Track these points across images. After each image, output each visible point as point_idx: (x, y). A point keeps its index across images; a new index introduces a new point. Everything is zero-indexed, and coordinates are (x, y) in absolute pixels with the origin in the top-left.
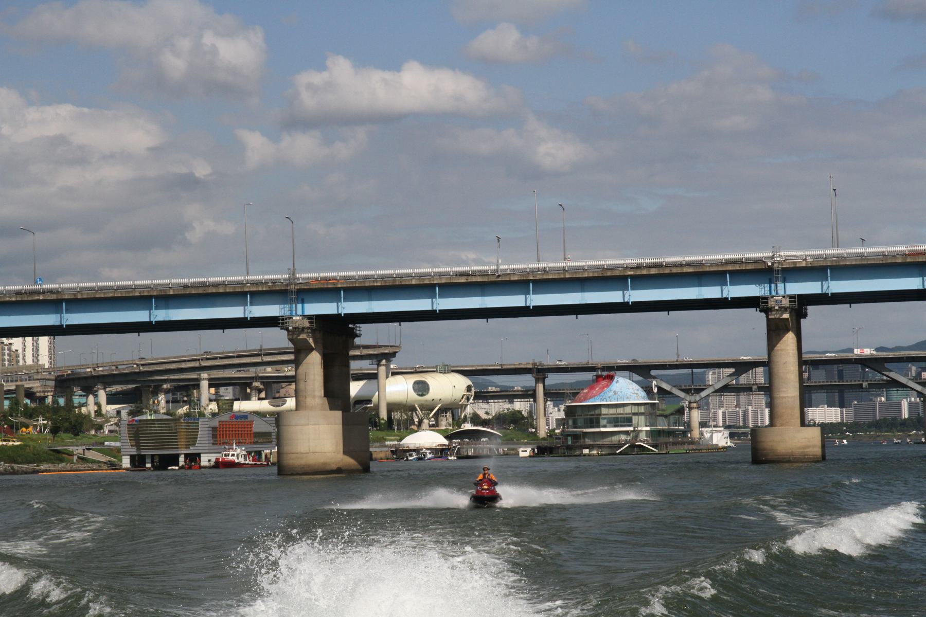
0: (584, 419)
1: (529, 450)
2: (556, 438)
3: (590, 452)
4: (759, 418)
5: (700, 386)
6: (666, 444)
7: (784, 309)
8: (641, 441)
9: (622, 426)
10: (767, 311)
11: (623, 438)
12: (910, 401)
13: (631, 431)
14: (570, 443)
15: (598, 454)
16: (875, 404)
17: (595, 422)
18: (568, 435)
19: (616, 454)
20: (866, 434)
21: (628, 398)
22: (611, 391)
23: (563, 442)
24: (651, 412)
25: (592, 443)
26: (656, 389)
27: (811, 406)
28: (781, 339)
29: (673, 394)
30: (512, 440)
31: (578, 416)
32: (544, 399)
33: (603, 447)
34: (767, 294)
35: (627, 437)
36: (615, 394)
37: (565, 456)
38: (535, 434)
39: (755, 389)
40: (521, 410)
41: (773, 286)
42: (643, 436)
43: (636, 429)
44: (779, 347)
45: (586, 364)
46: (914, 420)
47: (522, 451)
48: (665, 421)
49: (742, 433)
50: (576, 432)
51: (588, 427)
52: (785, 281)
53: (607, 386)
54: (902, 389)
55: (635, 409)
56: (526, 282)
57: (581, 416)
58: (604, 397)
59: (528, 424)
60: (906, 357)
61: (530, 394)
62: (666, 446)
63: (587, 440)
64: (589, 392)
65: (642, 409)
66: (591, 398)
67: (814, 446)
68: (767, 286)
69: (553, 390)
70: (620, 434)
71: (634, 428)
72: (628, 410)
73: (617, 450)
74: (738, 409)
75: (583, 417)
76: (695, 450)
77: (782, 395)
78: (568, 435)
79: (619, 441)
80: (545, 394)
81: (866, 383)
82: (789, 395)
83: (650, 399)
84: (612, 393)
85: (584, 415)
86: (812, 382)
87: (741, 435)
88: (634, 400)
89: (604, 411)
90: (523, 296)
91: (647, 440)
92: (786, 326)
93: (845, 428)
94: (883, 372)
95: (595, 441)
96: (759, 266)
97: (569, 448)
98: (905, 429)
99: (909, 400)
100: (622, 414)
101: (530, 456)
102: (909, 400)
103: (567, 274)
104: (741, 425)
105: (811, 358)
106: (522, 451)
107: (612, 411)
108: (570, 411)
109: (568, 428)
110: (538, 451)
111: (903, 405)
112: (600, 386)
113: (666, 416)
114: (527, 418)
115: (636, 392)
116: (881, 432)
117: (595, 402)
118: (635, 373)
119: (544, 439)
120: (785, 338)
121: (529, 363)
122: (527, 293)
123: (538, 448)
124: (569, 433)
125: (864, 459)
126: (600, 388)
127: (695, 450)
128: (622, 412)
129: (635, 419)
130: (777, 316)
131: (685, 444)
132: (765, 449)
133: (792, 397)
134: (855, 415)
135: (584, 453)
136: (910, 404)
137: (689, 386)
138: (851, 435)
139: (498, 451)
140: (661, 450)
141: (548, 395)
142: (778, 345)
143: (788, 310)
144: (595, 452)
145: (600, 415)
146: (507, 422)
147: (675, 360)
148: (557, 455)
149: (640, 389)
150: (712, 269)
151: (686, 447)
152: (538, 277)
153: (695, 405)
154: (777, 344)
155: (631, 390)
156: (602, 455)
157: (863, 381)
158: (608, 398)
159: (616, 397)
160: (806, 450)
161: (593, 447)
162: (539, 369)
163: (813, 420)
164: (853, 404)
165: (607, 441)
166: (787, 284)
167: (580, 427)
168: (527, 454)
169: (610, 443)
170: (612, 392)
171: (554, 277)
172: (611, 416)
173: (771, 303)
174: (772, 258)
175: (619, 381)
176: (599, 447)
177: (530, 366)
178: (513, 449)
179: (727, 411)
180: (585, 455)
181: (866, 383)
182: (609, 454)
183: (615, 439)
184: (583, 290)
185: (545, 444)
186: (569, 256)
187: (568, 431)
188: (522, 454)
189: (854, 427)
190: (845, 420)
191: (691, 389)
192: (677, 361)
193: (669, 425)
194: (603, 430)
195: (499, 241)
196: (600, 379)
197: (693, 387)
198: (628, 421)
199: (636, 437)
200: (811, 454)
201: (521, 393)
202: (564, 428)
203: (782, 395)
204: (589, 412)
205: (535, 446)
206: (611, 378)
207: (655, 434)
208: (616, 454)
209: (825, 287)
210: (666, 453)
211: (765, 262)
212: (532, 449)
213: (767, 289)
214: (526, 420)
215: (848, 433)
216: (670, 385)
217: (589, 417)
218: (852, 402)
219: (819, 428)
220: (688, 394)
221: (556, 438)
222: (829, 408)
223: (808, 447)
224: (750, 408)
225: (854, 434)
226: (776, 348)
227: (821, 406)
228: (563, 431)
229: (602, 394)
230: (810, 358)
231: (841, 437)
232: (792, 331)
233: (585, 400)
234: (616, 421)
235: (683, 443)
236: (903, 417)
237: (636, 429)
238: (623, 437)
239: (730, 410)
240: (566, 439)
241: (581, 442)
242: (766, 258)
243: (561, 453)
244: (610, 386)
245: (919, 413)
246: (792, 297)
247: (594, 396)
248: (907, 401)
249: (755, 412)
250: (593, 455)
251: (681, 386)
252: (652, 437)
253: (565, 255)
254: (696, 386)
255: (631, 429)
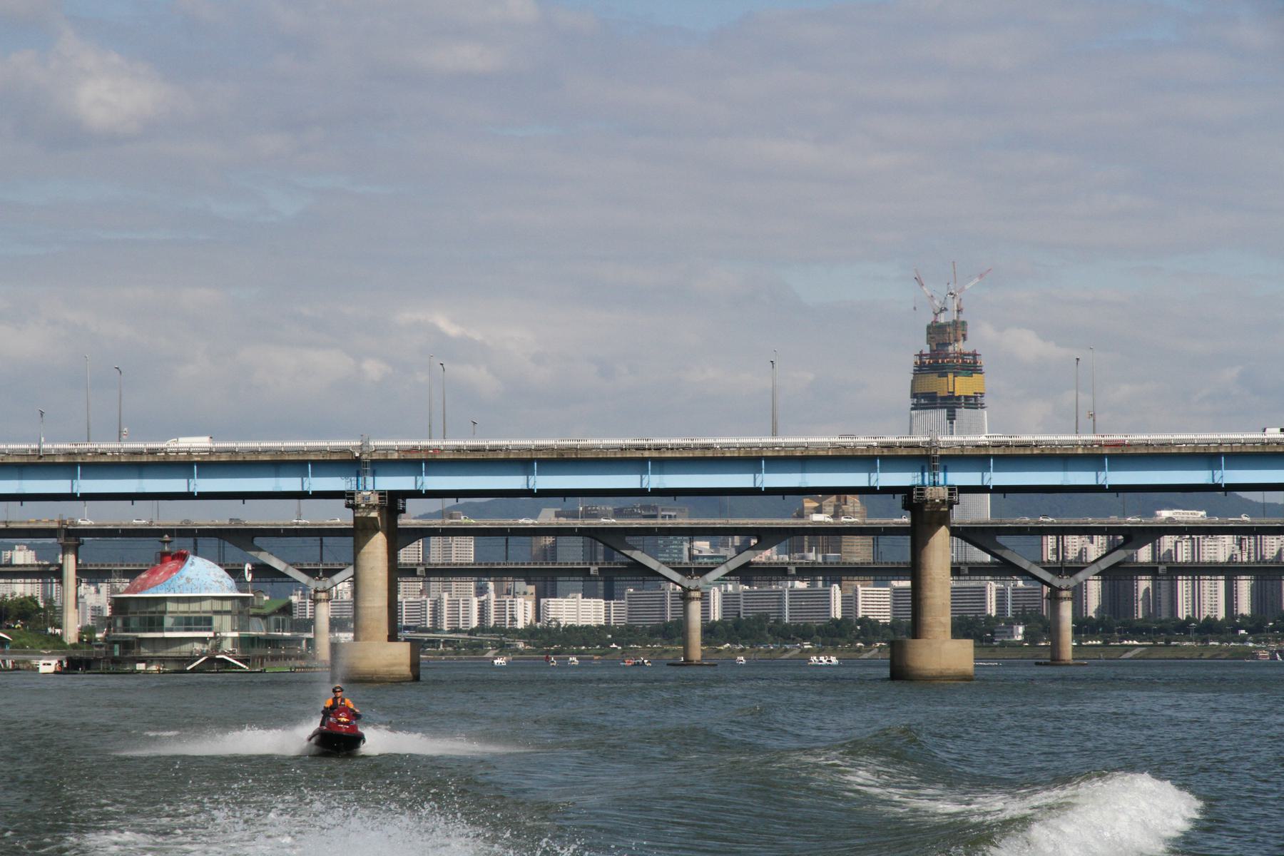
1: (54, 662)
2: (97, 646)
4: (461, 616)
5: (333, 564)
6: (262, 658)
9: (196, 630)
11: (197, 648)
12: (726, 591)
13: (211, 638)
14: (117, 653)
15: (159, 670)
16: (664, 597)
17: (156, 623)
18: (115, 642)
19: (186, 672)
21: (206, 588)
23: (106, 652)
24: (242, 609)
25: (151, 654)
27: (555, 597)
29: (289, 577)
30: (23, 646)
31: (132, 613)
32: (77, 579)
33: (167, 661)
34: (354, 488)
35: (204, 647)
36: (188, 582)
37: (108, 673)
38: (59, 638)
40: (36, 595)
41: (361, 479)
42: (227, 646)
43: (218, 634)
45: (149, 525)
46: (730, 625)
47: (44, 664)
48: (262, 623)
49: (429, 641)
50: (128, 637)
51: (145, 631)
52: (374, 474)
53: (177, 570)
54: (624, 578)
55: (217, 606)
56: (73, 466)
57: (136, 613)
58: (172, 586)
59: (45, 621)
60: (658, 528)
61: (52, 571)
63: (143, 650)
64: (149, 578)
65: (228, 606)
66: (152, 586)
67: (401, 664)
68: (354, 479)
69: (91, 565)
70: (194, 643)
71: (215, 634)
72: (206, 606)
73: (189, 665)
74: (424, 598)
75: (138, 615)
76: (304, 668)
77: (367, 604)
78: (115, 642)
79: (192, 652)
80: (78, 572)
81: (596, 568)
82: (376, 605)
83: (241, 591)
84: (183, 581)
86: (511, 564)
87: (428, 645)
88: (217, 592)
89: (171, 607)
91: (233, 652)
93: (610, 636)
94: (624, 552)
96: (345, 457)
97: (115, 661)
99: (723, 589)
100: (198, 612)
101: (55, 672)
102: (723, 589)
104: (428, 626)
106: (44, 664)
107: (183, 607)
108: (119, 606)
109: (114, 631)
110: (68, 664)
113: (264, 617)
114: (44, 610)
115: (220, 580)
116: (671, 644)
119: (74, 646)
121: (52, 521)
122: (73, 477)
123: (69, 660)
124: (116, 639)
127: (304, 668)
128: (197, 609)
129: (216, 620)
130: (364, 515)
133: (379, 607)
134: (631, 613)
136: (725, 596)
137: (316, 565)
138: (620, 648)
139: (5, 664)
140: (253, 666)
142: (366, 547)
144: (154, 668)
145: (164, 612)
149: (226, 575)
151: (291, 663)
152: (88, 460)
153: (323, 596)
154: (364, 545)
155: (213, 577)
156: (165, 672)
157: (591, 564)
158: (177, 589)
159: (189, 586)
160: (392, 669)
164: (626, 593)
165: (174, 652)
166: (376, 478)
167: (133, 631)
168: (51, 669)
169: (177, 655)
170: (184, 579)
172: (181, 615)
173: (358, 499)
175: (196, 564)
176: (160, 661)
177: (55, 525)
178: (24, 662)
179: (404, 600)
180: (139, 672)
181: (596, 568)
182: (176, 672)
183: (185, 649)
185: (77, 654)
186: (126, 429)
187: (115, 636)
188: (43, 669)
189: (626, 634)
190: (612, 621)
191: (318, 570)
193: (268, 630)
194: (168, 635)
195: (42, 415)
196: (168, 558)
197: (321, 567)
198: (206, 622)
199: (217, 647)
200: (397, 673)
201: (37, 569)
202: (109, 631)
203: (367, 604)
205: (63, 657)
206: (182, 558)
207: (246, 643)
208: (186, 672)
209: (419, 484)
210: (261, 672)
213: (354, 482)
215: (614, 646)
216: (285, 561)
218: (625, 589)
220: (314, 577)
221: (97, 646)
222: (585, 600)
223: (394, 665)
224: (446, 596)
225: (625, 646)
226: (362, 551)
227: (571, 595)
228: (107, 635)
230: (508, 524)
233: (143, 589)
234: (188, 622)
235: (287, 657)
236: (712, 618)
237: (218, 634)
238: (198, 647)
239: (411, 599)
240: (112, 648)
241: (134, 653)
242: (353, 447)
243: (104, 669)
244: (182, 571)
245: (739, 612)
246: (382, 493)
247: (157, 584)
248: (720, 590)
249: (454, 605)
250: (152, 673)
251: (302, 565)
252: (241, 646)
253: (120, 428)
254: (327, 565)
255: (211, 634)
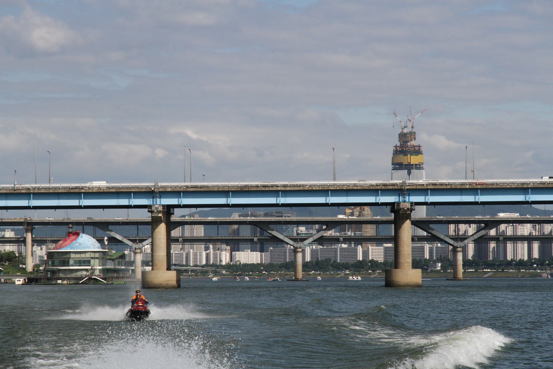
0: (59, 260)
1: (22, 280)
2: (41, 273)
3: (62, 282)
6: (112, 278)
7: (159, 212)
8: (96, 276)
9: (85, 266)
10: (152, 212)
11: (84, 274)
13: (90, 269)
14: (49, 276)
15: (67, 283)
18: (48, 271)
19: (79, 284)
20: (277, 273)
21: (88, 248)
22: (77, 243)
23: (45, 276)
24: (104, 257)
26: (107, 242)
27: (239, 251)
28: (158, 226)
30: (9, 273)
31: (55, 258)
32: (32, 244)
33: (71, 279)
34: (152, 204)
37: (45, 285)
38: (24, 269)
39: (181, 240)
41: (154, 199)
42: (97, 272)
43: (93, 268)
44: (157, 230)
47: (18, 281)
48: (112, 263)
50: (54, 269)
51: (61, 266)
52: (160, 198)
53: (75, 240)
54: (271, 243)
55: (93, 255)
57: (57, 258)
62: (112, 279)
63: (60, 274)
64: (63, 243)
65: (97, 255)
67: (173, 280)
68: (151, 200)
70: (83, 271)
71: (92, 267)
72: (88, 255)
77: (157, 254)
78: (48, 271)
79: (81, 275)
80: (33, 241)
81: (257, 238)
83: (103, 249)
84: (78, 244)
85: (59, 258)
86: (220, 237)
89: (72, 256)
90: (28, 201)
92: (161, 220)
93: (262, 268)
94: (268, 231)
95: (66, 275)
97: (48, 279)
98: (307, 269)
99: (311, 247)
100: (84, 258)
101: (22, 284)
102: (311, 247)
103: (50, 190)
104: (184, 264)
105: (220, 220)
106: (18, 281)
107: (78, 256)
109: (48, 266)
111: (306, 251)
112: (70, 239)
113: (113, 260)
115: (94, 244)
116: (288, 271)
117: (67, 250)
118: (98, 228)
119: (31, 273)
120: (161, 224)
121: (21, 218)
123: (28, 279)
124: (49, 270)
125: (190, 288)
126: (70, 241)
128: (84, 257)
129: (92, 261)
130: (156, 215)
131: (124, 278)
132: (148, 282)
133: (163, 256)
135: (58, 282)
136: (312, 251)
137: (135, 237)
138: (267, 273)
140: (108, 281)
141: (35, 241)
142: (157, 229)
143: (162, 212)
144: (65, 282)
146: (4, 260)
147: (126, 219)
148: (41, 284)
149: (97, 242)
150: (124, 191)
153: (138, 251)
154: (156, 229)
155: (90, 243)
156: (70, 284)
157: (254, 237)
158: (75, 248)
159: (80, 247)
161: (64, 279)
162: (28, 222)
163: (239, 261)
164: (269, 249)
165: (74, 275)
166: (161, 199)
167: (56, 266)
168: (21, 283)
169: (75, 276)
171: (44, 192)
173: (153, 209)
174: (154, 186)
176: (68, 279)
178: (9, 279)
179: (174, 253)
180: (59, 284)
181: (257, 238)
182: (75, 284)
183: (79, 274)
184: (59, 199)
185: (32, 276)
187: (48, 268)
188: (17, 283)
189: (269, 267)
190: (263, 262)
192: (127, 220)
193: (115, 265)
194: (71, 268)
196: (71, 234)
197: (138, 238)
198: (87, 262)
199: (92, 273)
200: (171, 284)
201: (15, 239)
202: (46, 266)
203: (157, 254)
204: (62, 256)
205: (26, 278)
206: (77, 234)
207: (105, 271)
208: (79, 284)
209: (180, 202)
210: (111, 284)
211: (151, 188)
212: (24, 279)
213: (152, 201)
214: (17, 259)
215: (264, 272)
216: (122, 236)
217: (62, 259)
219: (175, 271)
220: (134, 243)
221: (41, 273)
222: (252, 252)
223: (169, 281)
224: (191, 251)
228: (45, 268)
229: (72, 244)
231: (259, 275)
232: (164, 223)
233: (60, 248)
234: (80, 262)
236: (306, 260)
237: (93, 268)
238: (84, 273)
239: (177, 252)
240: (47, 274)
242: (151, 186)
244: (77, 240)
245: (318, 257)
246: (164, 206)
247: (66, 246)
248: (310, 248)
249: (195, 255)
250: (64, 284)
251: (129, 237)
255: (90, 268)
